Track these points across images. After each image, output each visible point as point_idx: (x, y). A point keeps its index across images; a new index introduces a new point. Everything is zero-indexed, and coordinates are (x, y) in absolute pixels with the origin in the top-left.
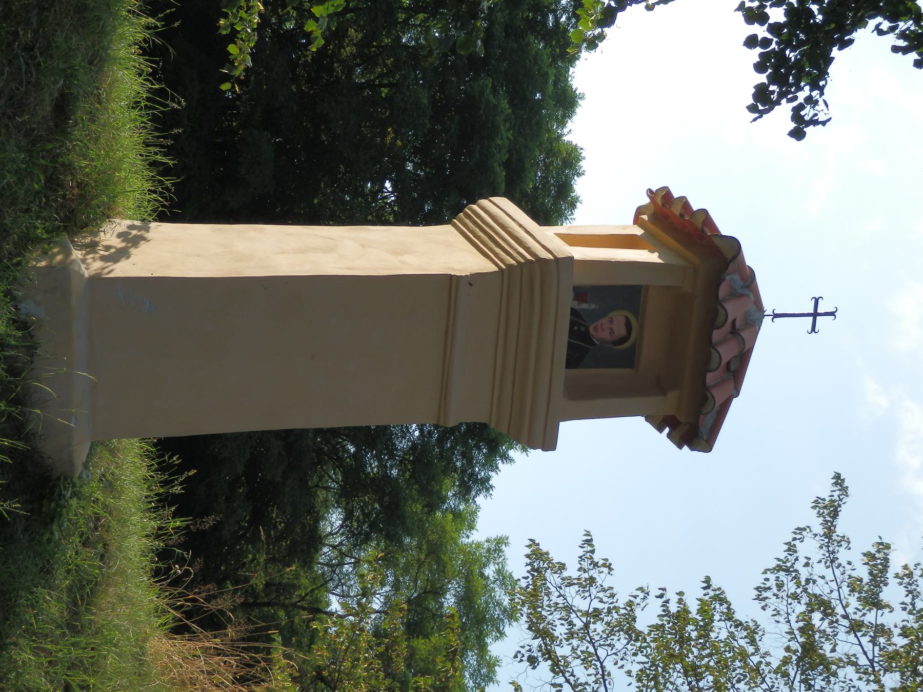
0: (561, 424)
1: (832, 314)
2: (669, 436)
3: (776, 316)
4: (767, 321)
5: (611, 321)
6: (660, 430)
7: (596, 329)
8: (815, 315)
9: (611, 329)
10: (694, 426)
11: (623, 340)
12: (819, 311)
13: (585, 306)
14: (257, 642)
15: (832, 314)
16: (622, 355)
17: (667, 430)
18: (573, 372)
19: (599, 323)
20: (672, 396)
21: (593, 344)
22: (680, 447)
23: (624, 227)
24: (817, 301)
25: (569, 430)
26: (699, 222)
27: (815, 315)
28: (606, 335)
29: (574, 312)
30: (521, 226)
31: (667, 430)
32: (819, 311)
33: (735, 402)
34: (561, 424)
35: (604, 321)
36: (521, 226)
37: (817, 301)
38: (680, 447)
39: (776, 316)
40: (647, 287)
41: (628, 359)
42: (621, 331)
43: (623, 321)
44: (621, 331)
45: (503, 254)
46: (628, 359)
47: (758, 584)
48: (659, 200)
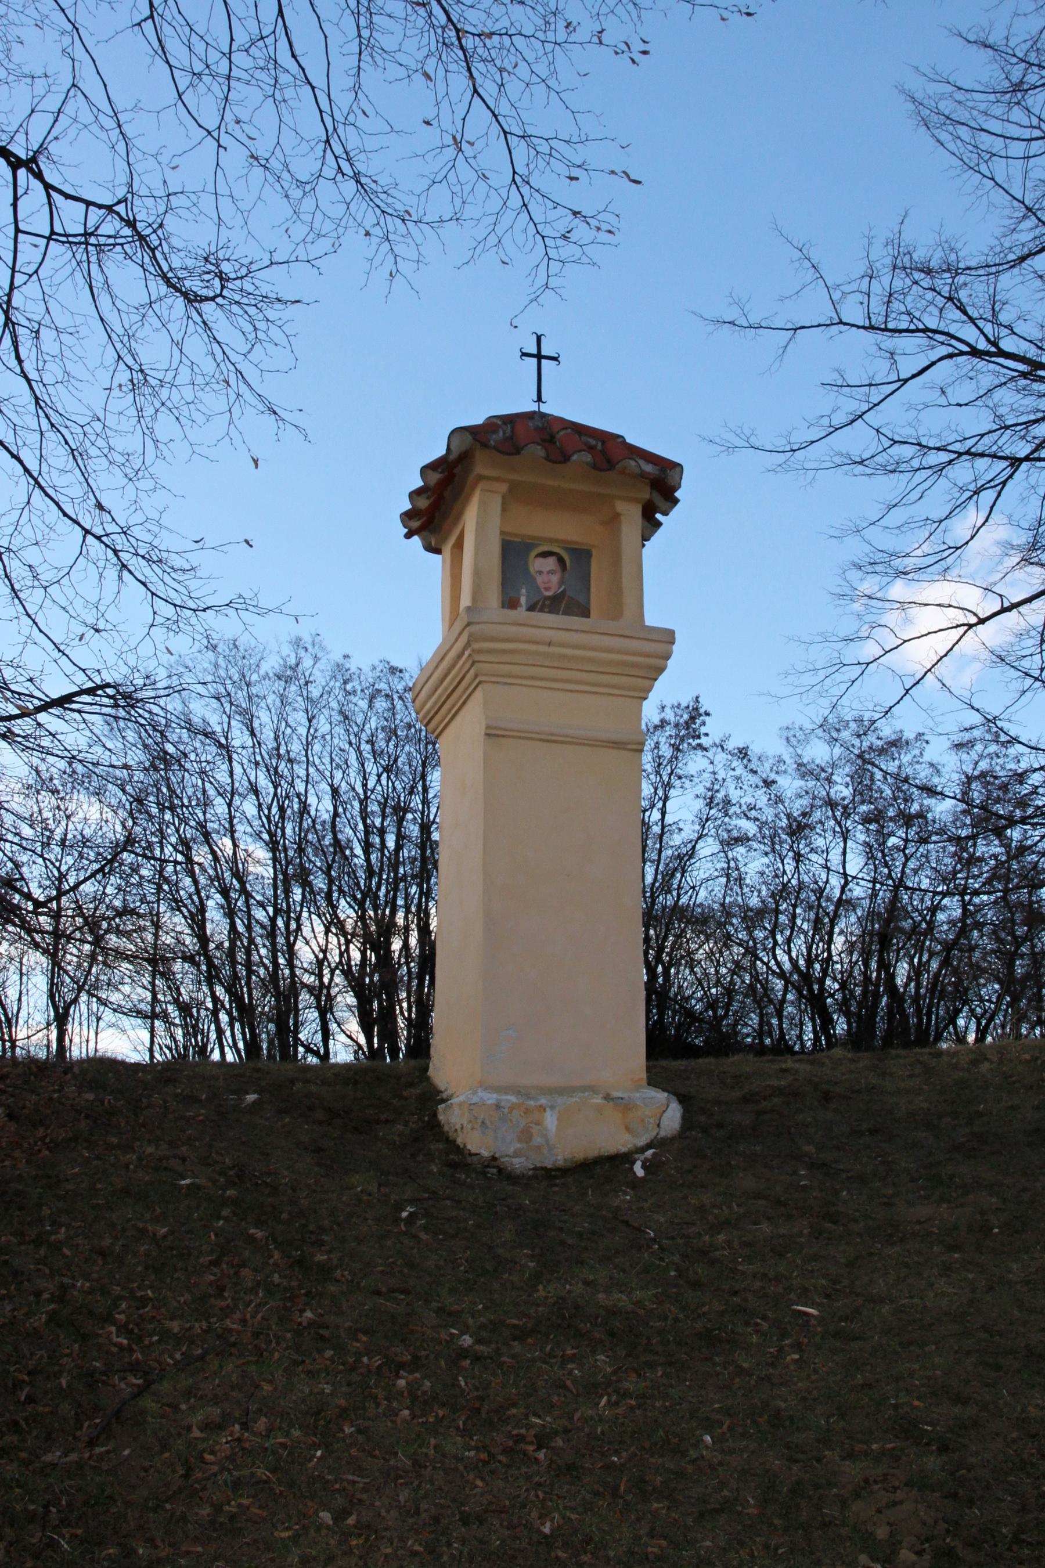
0: (649, 622)
1: (539, 339)
2: (665, 513)
3: (539, 399)
4: (545, 409)
5: (540, 572)
6: (659, 524)
7: (547, 589)
8: (539, 357)
9: (549, 572)
10: (658, 485)
11: (561, 560)
12: (535, 352)
13: (523, 600)
14: (506, 1093)
15: (539, 339)
16: (576, 560)
17: (658, 516)
18: (594, 613)
19: (542, 586)
20: (621, 506)
21: (564, 591)
22: (676, 501)
23: (444, 561)
24: (524, 354)
25: (653, 617)
26: (435, 477)
27: (539, 357)
28: (555, 579)
29: (531, 608)
30: (437, 667)
31: (658, 516)
32: (535, 352)
33: (628, 440)
34: (649, 622)
35: (539, 580)
36: (437, 667)
37: (524, 354)
38: (676, 501)
39: (539, 399)
40: (502, 533)
41: (582, 555)
42: (551, 563)
43: (540, 560)
44: (551, 563)
45: (453, 673)
46: (582, 555)
47: (755, 750)
48: (415, 524)
